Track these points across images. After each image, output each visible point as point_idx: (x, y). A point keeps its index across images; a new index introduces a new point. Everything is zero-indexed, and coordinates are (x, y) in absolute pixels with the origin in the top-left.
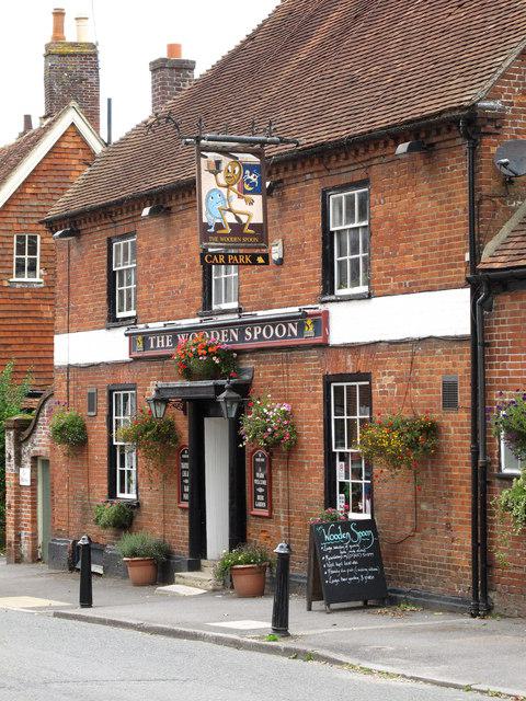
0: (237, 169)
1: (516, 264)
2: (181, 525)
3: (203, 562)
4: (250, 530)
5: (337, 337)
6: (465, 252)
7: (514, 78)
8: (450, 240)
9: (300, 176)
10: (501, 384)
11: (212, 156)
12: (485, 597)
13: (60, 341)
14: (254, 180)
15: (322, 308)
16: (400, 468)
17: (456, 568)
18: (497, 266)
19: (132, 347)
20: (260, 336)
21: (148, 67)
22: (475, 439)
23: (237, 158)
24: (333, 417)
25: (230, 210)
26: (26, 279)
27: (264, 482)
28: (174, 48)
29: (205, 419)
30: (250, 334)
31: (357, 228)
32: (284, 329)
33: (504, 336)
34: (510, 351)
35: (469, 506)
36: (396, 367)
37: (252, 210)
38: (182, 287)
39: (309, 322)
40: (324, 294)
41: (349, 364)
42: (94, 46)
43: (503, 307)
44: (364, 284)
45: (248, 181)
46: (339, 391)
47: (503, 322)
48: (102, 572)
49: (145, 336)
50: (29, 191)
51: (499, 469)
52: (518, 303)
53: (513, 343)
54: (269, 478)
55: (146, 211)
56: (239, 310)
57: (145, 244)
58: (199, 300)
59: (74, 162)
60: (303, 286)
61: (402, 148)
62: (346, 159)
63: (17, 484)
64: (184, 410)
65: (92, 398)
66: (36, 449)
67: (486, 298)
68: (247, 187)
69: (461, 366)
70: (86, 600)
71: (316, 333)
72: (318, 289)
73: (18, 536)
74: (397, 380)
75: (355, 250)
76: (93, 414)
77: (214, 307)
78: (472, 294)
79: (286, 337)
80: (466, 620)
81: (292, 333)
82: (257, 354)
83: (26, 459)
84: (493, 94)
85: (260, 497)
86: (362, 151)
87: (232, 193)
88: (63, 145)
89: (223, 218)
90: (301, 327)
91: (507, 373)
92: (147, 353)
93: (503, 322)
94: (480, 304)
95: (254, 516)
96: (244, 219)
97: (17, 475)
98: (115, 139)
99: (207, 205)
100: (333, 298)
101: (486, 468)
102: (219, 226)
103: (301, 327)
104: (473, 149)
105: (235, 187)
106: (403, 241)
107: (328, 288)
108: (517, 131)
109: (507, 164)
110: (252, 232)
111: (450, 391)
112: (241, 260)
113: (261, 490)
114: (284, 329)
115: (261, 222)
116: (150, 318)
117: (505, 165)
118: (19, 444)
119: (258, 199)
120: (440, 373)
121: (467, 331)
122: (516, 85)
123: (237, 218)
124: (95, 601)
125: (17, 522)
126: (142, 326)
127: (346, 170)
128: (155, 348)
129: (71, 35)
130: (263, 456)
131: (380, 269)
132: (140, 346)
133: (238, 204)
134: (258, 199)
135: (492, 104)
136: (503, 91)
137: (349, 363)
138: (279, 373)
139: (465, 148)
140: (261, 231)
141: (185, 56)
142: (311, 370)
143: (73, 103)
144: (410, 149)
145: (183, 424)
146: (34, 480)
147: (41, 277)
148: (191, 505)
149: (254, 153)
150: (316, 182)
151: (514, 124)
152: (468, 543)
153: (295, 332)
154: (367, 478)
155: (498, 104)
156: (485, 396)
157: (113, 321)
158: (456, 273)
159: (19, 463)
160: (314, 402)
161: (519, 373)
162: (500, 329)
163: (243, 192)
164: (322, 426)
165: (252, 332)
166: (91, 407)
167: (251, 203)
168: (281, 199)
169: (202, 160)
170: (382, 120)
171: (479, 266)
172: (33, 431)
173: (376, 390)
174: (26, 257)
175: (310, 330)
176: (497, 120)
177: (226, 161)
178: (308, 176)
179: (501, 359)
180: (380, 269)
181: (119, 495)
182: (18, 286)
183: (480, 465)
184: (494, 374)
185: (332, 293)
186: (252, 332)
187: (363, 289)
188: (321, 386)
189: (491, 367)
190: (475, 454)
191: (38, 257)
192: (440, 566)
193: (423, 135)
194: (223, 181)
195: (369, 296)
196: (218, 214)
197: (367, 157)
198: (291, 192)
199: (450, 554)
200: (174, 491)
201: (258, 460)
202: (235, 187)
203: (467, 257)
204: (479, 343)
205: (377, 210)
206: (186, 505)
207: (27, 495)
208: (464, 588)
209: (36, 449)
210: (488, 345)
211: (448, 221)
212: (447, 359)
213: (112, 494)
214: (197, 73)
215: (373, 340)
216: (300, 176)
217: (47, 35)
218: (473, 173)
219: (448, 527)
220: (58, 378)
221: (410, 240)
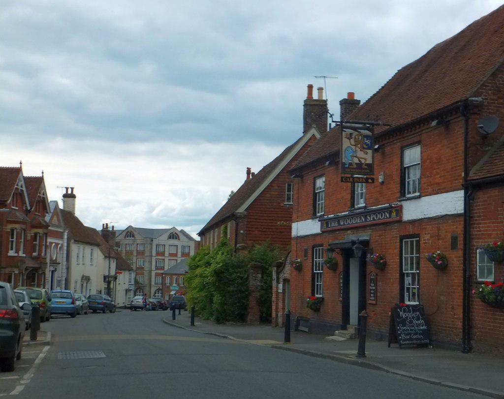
0: (360, 137)
1: (485, 176)
3: (348, 326)
6: (462, 172)
7: (488, 86)
8: (456, 167)
9: (391, 142)
10: (478, 237)
11: (349, 131)
12: (469, 343)
13: (295, 226)
14: (369, 143)
15: (399, 204)
17: (456, 328)
18: (478, 177)
20: (373, 218)
21: (339, 103)
22: (465, 264)
23: (360, 132)
24: (404, 256)
25: (356, 157)
27: (374, 288)
28: (351, 95)
29: (351, 259)
30: (369, 218)
32: (383, 215)
33: (479, 213)
34: (482, 220)
35: (462, 298)
36: (431, 231)
37: (367, 157)
39: (394, 211)
41: (411, 230)
42: (325, 101)
43: (479, 198)
44: (418, 192)
45: (366, 143)
47: (479, 205)
48: (307, 331)
51: (476, 278)
52: (486, 196)
53: (483, 216)
54: (376, 285)
55: (327, 163)
56: (365, 207)
58: (349, 203)
60: (391, 194)
61: (434, 123)
62: (411, 131)
63: (277, 291)
65: (306, 251)
66: (285, 275)
67: (471, 193)
68: (365, 146)
69: (459, 228)
70: (287, 339)
71: (397, 215)
72: (398, 195)
73: (277, 315)
74: (431, 237)
76: (306, 258)
77: (356, 207)
78: (465, 193)
80: (460, 354)
81: (386, 216)
82: (372, 228)
83: (281, 280)
84: (477, 94)
85: (372, 295)
86: (418, 127)
87: (357, 149)
88: (309, 144)
89: (352, 160)
90: (390, 213)
91: (480, 231)
93: (479, 205)
94: (469, 197)
95: (370, 304)
96: (363, 161)
97: (277, 288)
99: (345, 154)
100: (404, 198)
101: (470, 277)
102: (350, 164)
103: (390, 213)
104: (467, 121)
105: (359, 146)
106: (435, 169)
107: (403, 192)
108: (490, 113)
109: (482, 127)
110: (366, 167)
111: (454, 240)
112: (361, 180)
113: (372, 292)
114: (383, 215)
115: (371, 162)
117: (481, 128)
118: (278, 273)
119: (370, 152)
122: (490, 90)
123: (360, 161)
125: (277, 308)
126: (326, 217)
127: (412, 137)
128: (331, 227)
129: (315, 96)
131: (424, 183)
132: (325, 225)
133: (360, 154)
134: (370, 152)
135: (477, 99)
136: (482, 93)
138: (382, 236)
139: (463, 122)
140: (370, 167)
141: (356, 98)
142: (394, 232)
143: (314, 126)
144: (438, 123)
145: (340, 260)
146: (284, 290)
148: (343, 299)
149: (367, 129)
150: (399, 144)
151: (488, 109)
152: (461, 316)
153: (388, 216)
154: (418, 285)
155: (480, 99)
157: (314, 216)
158: (458, 183)
159: (278, 282)
160: (396, 249)
161: (486, 230)
162: (478, 209)
163: (362, 149)
164: (399, 260)
165: (370, 217)
167: (366, 153)
168: (383, 154)
170: (426, 111)
171: (469, 178)
172: (284, 267)
175: (394, 214)
176: (479, 107)
178: (395, 142)
179: (478, 224)
180: (424, 183)
181: (316, 296)
182: (288, 206)
183: (467, 277)
184: (475, 232)
186: (370, 217)
187: (417, 194)
188: (398, 241)
189: (473, 228)
190: (465, 271)
192: (449, 327)
193: (444, 117)
194: (353, 143)
195: (419, 197)
196: (350, 158)
197: (420, 130)
198: (387, 150)
199: (453, 321)
201: (371, 277)
202: (359, 146)
203: (463, 174)
204: (467, 216)
206: (341, 299)
207: (281, 296)
208: (459, 339)
209: (285, 275)
210: (472, 217)
211: (455, 158)
212: (453, 225)
213: (313, 294)
214: (362, 103)
216: (391, 142)
217: (305, 96)
218: (467, 133)
219: (453, 308)
220: (293, 242)
221: (438, 168)
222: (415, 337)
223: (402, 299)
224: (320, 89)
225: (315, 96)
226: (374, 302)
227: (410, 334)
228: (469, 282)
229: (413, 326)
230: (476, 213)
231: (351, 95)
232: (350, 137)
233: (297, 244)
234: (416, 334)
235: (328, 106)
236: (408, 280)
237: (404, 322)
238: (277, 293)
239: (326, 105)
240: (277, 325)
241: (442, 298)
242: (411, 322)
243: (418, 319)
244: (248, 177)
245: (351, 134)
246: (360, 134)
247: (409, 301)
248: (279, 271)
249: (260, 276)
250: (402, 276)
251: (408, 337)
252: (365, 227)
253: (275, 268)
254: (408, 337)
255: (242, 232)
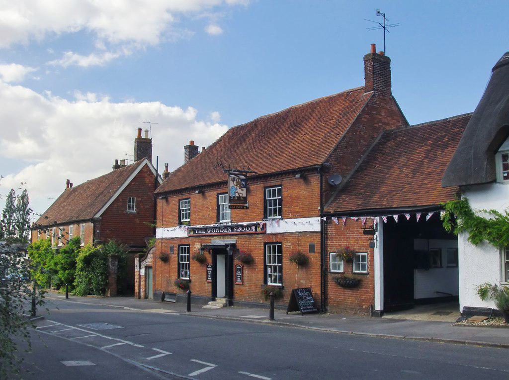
2: (209, 287)
3: (216, 298)
4: (235, 289)
5: (269, 231)
6: (318, 206)
11: (233, 176)
16: (75, 278)
19: (189, 233)
20: (215, 232)
22: (322, 261)
26: (131, 211)
27: (208, 269)
28: (192, 142)
29: (218, 256)
31: (277, 199)
33: (332, 232)
37: (243, 193)
38: (209, 215)
40: (264, 218)
42: (150, 140)
46: (182, 248)
49: (194, 230)
50: (133, 184)
51: (330, 270)
53: (335, 234)
55: (197, 192)
57: (194, 202)
58: (215, 219)
59: (146, 175)
61: (298, 176)
64: (209, 252)
69: (317, 240)
70: (189, 309)
72: (262, 217)
73: (139, 291)
75: (275, 205)
79: (250, 231)
83: (143, 266)
88: (144, 170)
92: (195, 235)
93: (332, 227)
96: (241, 195)
97: (140, 272)
98: (171, 170)
102: (234, 197)
113: (239, 277)
116: (196, 224)
119: (245, 189)
120: (308, 242)
121: (320, 230)
124: (191, 310)
129: (143, 136)
130: (240, 266)
131: (286, 211)
133: (239, 191)
137: (274, 239)
142: (260, 239)
145: (209, 258)
147: (136, 210)
150: (262, 185)
156: (325, 249)
159: (140, 268)
160: (260, 250)
163: (241, 187)
166: (171, 251)
169: (230, 177)
173: (284, 247)
174: (131, 204)
177: (236, 178)
180: (286, 211)
185: (267, 218)
190: (322, 266)
191: (135, 204)
200: (205, 277)
203: (319, 208)
204: (323, 232)
205: (285, 193)
207: (143, 278)
212: (311, 238)
213: (179, 277)
215: (283, 232)
217: (136, 136)
222: (309, 307)
223: (266, 281)
224: (147, 131)
225: (143, 136)
226: (241, 283)
227: (306, 306)
228: (324, 272)
229: (307, 301)
230: (330, 232)
231: (192, 142)
232: (233, 180)
233: (162, 243)
234: (309, 306)
235: (152, 143)
236: (269, 270)
237: (301, 298)
238: (140, 276)
239: (151, 142)
240: (140, 298)
241: (302, 281)
242: (305, 298)
243: (309, 296)
244: (68, 187)
245: (234, 178)
246: (239, 178)
247: (271, 282)
248: (141, 260)
249: (117, 263)
250: (266, 268)
251: (305, 308)
252: (233, 235)
253: (138, 258)
254: (305, 308)
255: (98, 231)
